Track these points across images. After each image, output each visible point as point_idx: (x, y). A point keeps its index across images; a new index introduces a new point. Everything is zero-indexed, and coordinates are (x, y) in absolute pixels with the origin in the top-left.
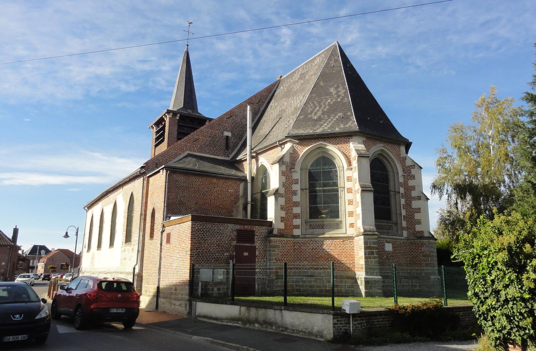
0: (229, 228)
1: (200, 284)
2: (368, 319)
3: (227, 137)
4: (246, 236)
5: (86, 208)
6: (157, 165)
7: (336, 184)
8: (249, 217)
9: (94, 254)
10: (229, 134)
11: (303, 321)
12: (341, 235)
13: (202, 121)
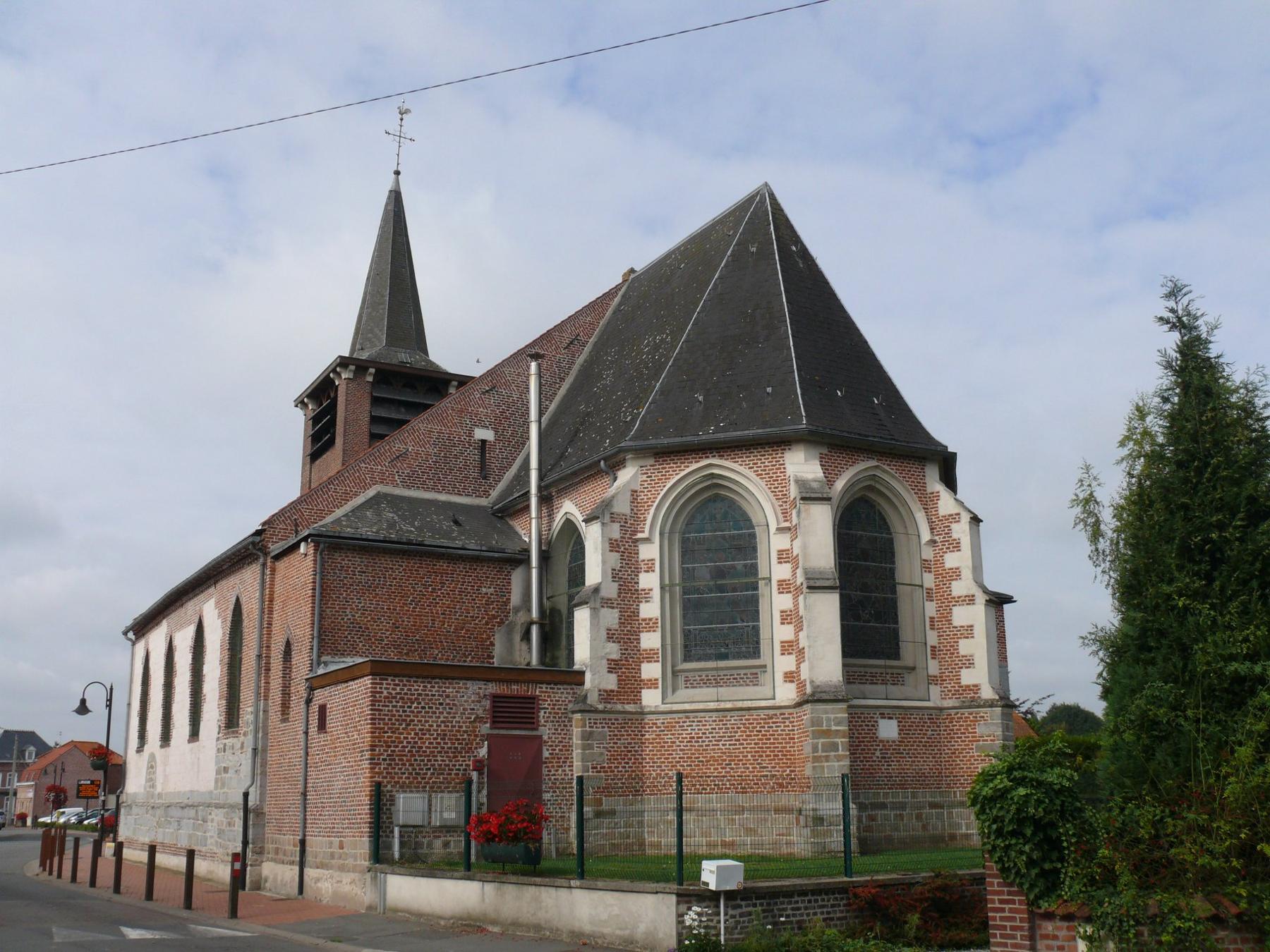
0: (470, 691)
1: (396, 830)
2: (768, 904)
3: (484, 442)
4: (513, 712)
5: (131, 635)
6: (296, 525)
7: (753, 570)
8: (534, 661)
9: (152, 757)
10: (486, 434)
11: (616, 911)
12: (763, 704)
13: (437, 384)
